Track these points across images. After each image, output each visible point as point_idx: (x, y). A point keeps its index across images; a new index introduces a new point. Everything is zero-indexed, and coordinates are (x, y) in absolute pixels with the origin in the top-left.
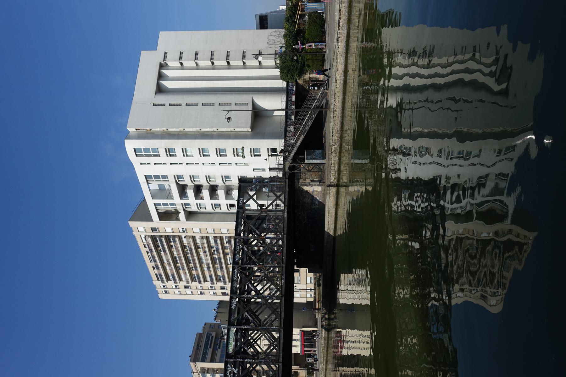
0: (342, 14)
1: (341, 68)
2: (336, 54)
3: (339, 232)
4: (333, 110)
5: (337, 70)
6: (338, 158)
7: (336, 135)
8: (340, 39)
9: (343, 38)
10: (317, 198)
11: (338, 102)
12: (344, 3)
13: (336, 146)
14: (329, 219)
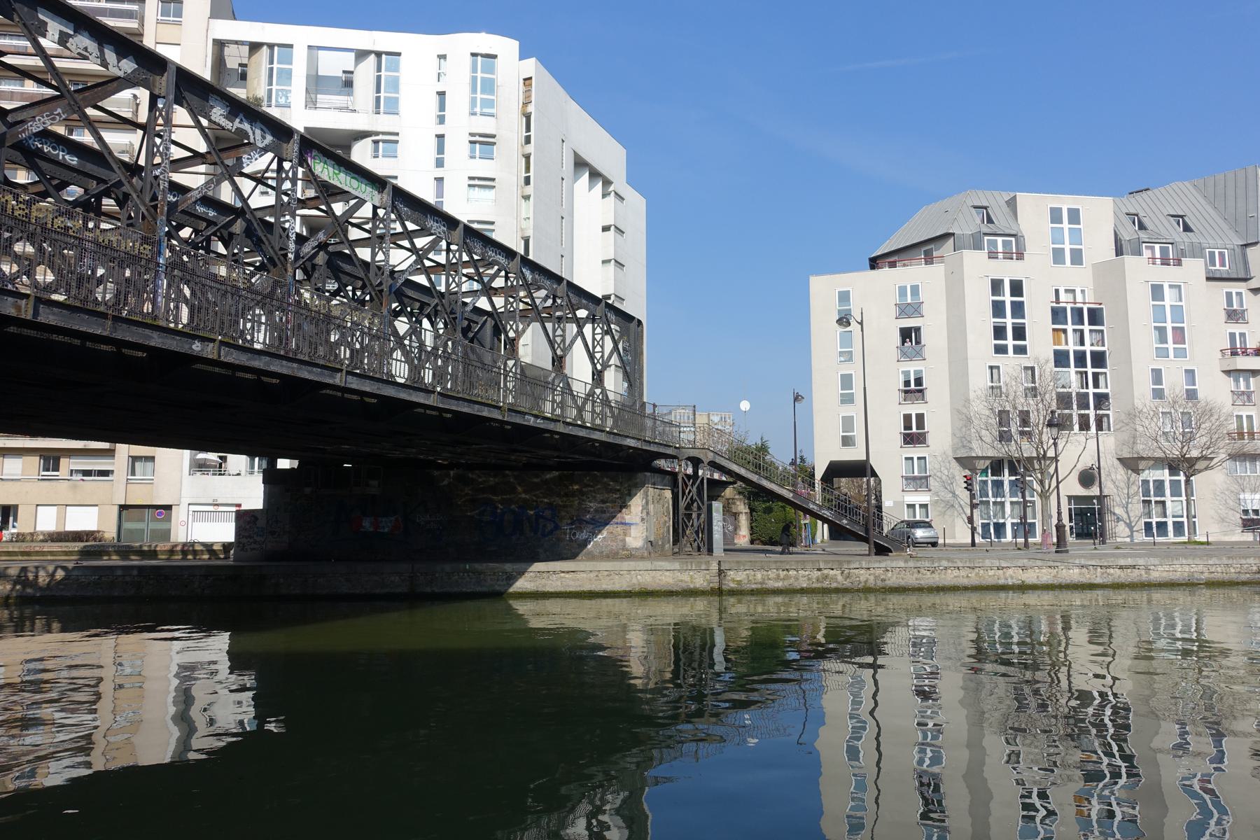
0: (1129, 571)
1: (1030, 577)
2: (1056, 564)
3: (522, 607)
4: (936, 565)
5: (1024, 568)
6: (805, 585)
7: (872, 578)
8: (1084, 570)
9: (1088, 576)
10: (600, 536)
11: (955, 577)
12: (1146, 573)
13: (840, 578)
14: (584, 575)
